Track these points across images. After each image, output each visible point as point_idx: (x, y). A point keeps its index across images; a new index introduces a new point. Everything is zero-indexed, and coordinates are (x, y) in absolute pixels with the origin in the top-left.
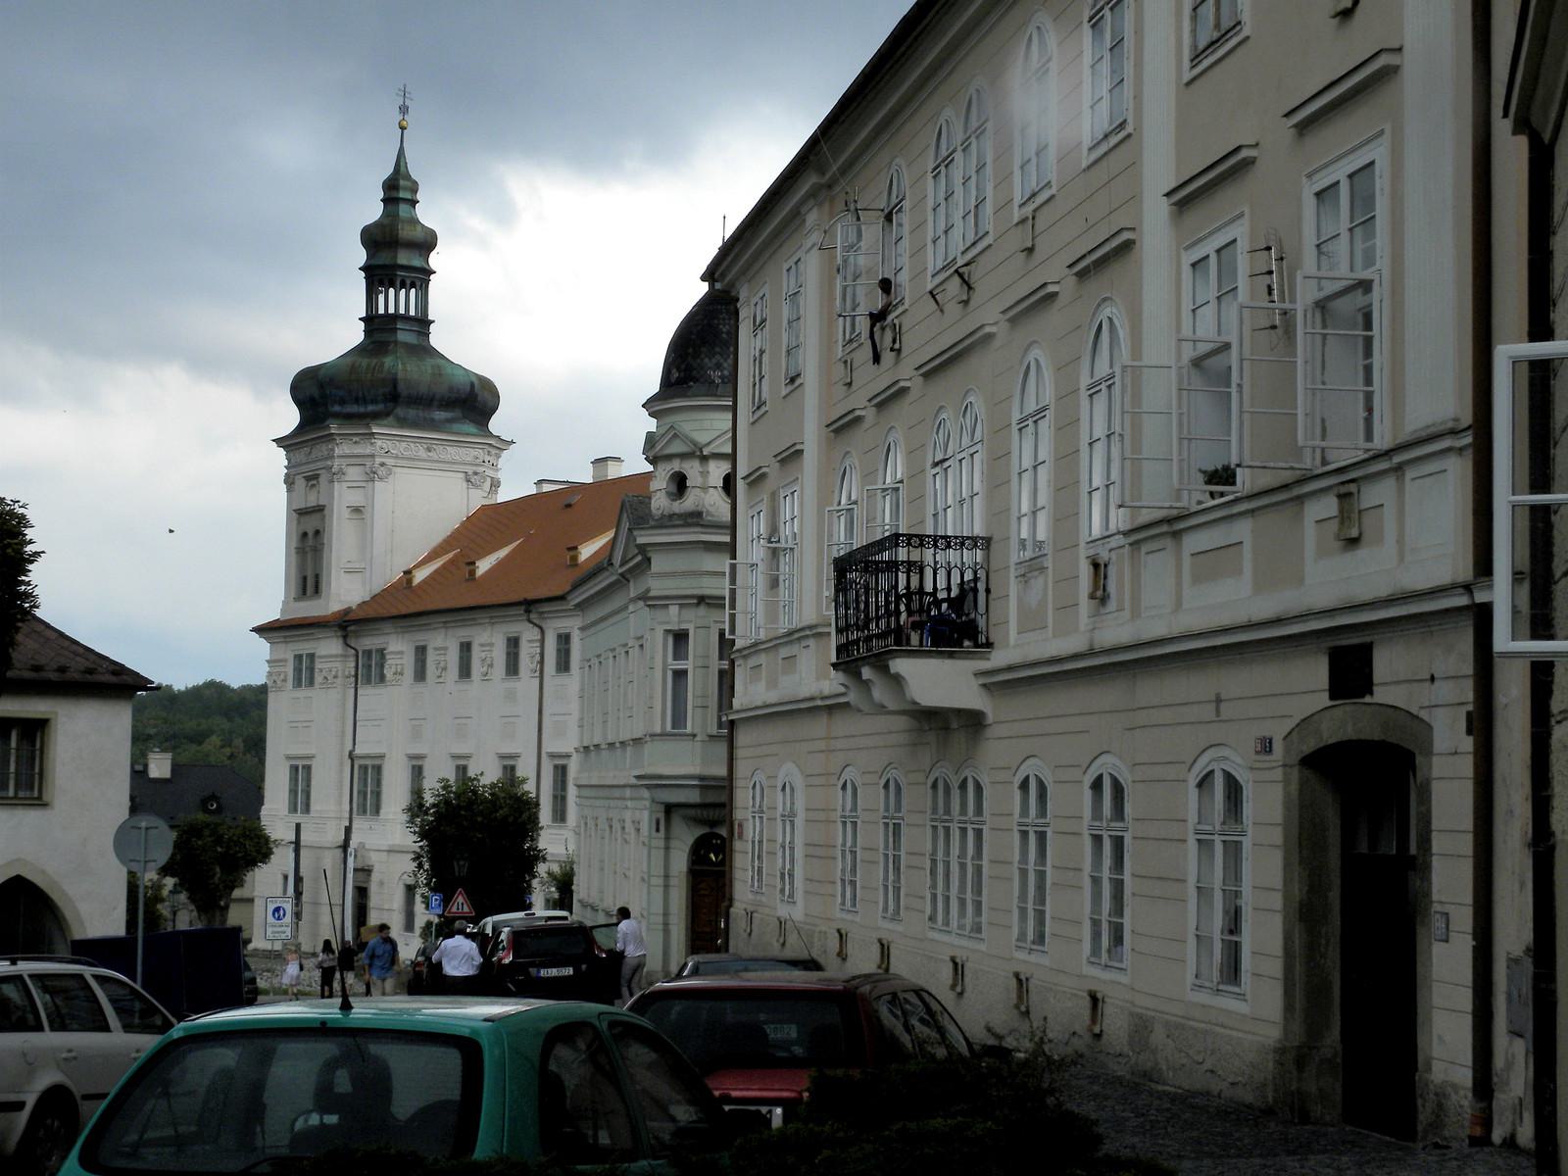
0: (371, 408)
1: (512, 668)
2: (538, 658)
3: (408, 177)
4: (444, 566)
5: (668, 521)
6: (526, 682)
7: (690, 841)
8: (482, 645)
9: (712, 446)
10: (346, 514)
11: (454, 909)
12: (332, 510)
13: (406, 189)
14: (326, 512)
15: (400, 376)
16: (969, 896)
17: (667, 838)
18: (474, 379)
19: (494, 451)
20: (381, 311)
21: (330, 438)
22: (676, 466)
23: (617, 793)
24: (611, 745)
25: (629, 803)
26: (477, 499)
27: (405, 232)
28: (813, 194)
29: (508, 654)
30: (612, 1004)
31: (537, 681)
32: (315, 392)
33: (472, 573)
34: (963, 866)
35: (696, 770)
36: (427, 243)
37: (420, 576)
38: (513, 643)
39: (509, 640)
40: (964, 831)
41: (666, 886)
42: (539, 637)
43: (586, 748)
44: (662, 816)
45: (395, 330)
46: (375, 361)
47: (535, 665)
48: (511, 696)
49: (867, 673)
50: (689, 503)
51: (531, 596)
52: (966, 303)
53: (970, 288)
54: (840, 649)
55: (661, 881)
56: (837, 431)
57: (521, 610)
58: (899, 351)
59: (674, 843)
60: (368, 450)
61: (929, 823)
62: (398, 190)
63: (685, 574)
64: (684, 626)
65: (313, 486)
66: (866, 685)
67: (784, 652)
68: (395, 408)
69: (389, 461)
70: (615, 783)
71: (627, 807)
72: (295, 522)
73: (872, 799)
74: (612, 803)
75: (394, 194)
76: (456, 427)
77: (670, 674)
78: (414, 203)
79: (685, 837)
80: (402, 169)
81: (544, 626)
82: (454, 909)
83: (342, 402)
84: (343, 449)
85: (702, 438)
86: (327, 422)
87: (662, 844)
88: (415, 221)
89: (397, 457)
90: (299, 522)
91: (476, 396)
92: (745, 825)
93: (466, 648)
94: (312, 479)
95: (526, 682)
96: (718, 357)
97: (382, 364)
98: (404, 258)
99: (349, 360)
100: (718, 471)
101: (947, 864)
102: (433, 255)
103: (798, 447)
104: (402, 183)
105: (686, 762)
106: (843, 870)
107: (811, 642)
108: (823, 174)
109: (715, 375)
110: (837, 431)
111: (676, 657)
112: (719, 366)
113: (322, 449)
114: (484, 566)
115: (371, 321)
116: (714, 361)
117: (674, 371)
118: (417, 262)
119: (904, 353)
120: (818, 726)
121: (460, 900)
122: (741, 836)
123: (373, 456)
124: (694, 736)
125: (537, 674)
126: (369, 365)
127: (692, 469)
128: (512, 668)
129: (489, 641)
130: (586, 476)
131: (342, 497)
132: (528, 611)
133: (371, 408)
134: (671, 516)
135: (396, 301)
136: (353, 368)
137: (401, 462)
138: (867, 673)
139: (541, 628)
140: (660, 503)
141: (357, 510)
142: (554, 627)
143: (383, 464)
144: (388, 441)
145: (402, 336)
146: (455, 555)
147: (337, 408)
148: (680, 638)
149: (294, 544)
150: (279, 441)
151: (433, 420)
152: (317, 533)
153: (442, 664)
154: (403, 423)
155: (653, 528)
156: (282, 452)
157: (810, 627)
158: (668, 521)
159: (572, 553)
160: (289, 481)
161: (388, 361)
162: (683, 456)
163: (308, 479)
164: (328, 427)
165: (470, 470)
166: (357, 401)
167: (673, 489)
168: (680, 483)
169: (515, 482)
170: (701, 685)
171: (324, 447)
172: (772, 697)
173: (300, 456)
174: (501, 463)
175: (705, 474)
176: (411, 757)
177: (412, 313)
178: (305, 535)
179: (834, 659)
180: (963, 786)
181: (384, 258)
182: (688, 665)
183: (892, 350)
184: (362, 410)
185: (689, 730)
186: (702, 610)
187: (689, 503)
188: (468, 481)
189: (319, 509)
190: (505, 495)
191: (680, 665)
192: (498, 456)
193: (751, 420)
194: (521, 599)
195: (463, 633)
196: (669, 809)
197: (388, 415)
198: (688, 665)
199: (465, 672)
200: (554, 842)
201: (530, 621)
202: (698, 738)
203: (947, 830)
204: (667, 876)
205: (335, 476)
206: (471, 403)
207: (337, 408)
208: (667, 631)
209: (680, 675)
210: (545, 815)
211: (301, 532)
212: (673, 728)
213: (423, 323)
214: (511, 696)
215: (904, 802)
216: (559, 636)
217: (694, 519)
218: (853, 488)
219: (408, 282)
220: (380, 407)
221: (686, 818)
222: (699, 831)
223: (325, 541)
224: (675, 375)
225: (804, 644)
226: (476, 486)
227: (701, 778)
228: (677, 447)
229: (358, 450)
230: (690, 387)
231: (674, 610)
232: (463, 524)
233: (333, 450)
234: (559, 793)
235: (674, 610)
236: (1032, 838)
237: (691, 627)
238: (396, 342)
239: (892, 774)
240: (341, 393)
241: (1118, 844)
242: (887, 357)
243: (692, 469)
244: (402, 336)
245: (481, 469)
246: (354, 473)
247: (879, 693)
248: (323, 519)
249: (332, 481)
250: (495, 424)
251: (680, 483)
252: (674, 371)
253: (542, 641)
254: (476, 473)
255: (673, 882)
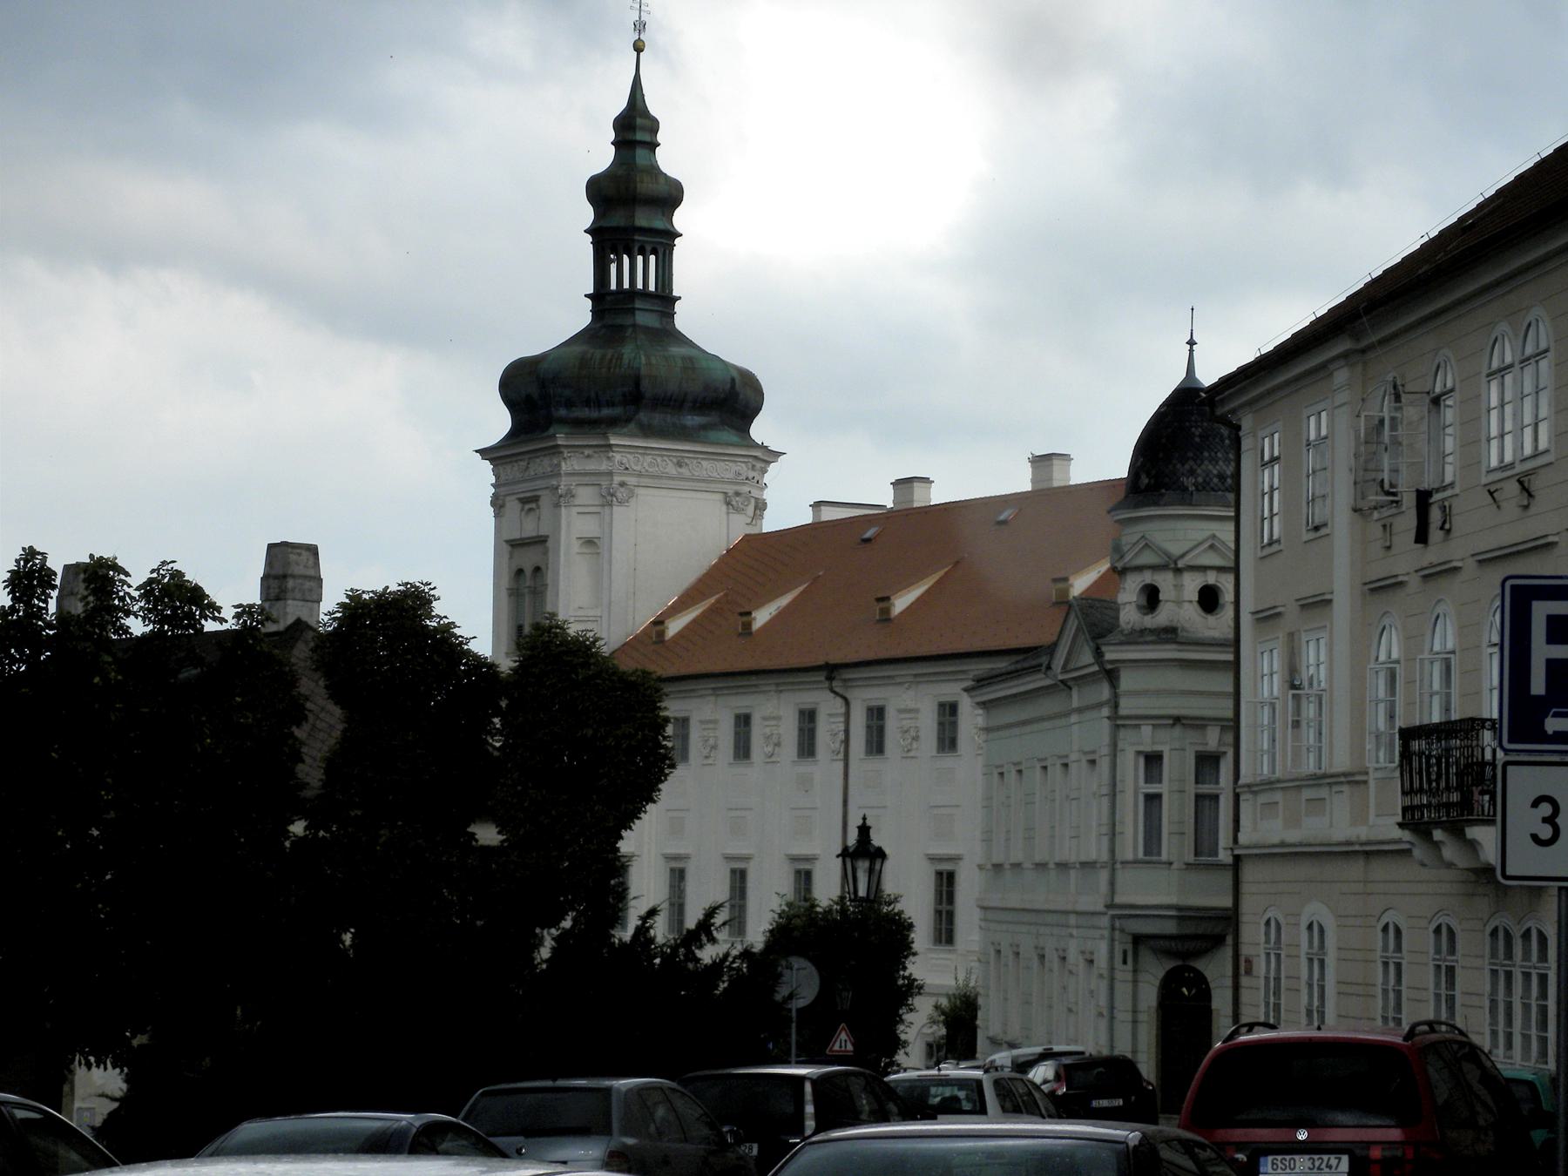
0: (606, 412)
1: (807, 747)
2: (841, 736)
3: (645, 113)
4: (703, 615)
5: (1138, 636)
6: (825, 767)
7: (1161, 974)
8: (765, 719)
9: (1187, 558)
10: (576, 547)
11: (836, 1047)
12: (558, 541)
13: (643, 129)
14: (550, 544)
15: (643, 371)
16: (1534, 1032)
17: (1135, 971)
18: (735, 374)
19: (759, 465)
20: (613, 286)
21: (555, 450)
22: (1147, 578)
23: (1049, 918)
24: (1041, 866)
25: (1074, 932)
26: (739, 529)
27: (645, 186)
28: (1345, 356)
29: (801, 730)
30: (1156, 1123)
31: (841, 765)
32: (534, 391)
33: (747, 626)
34: (1526, 1007)
35: (1173, 900)
36: (671, 196)
37: (674, 627)
38: (808, 718)
39: (802, 713)
40: (1527, 976)
41: (1135, 1022)
42: (843, 710)
43: (998, 867)
44: (1129, 947)
45: (632, 311)
46: (610, 352)
47: (838, 745)
48: (805, 784)
49: (1438, 835)
50: (1162, 617)
51: (835, 658)
52: (1526, 507)
53: (1530, 495)
54: (1405, 810)
55: (1129, 1017)
56: (1373, 590)
57: (821, 677)
58: (1449, 531)
59: (1142, 977)
60: (604, 467)
61: (1488, 968)
62: (635, 129)
63: (1158, 693)
64: (1157, 748)
65: (531, 510)
66: (1437, 846)
67: (1307, 794)
68: (637, 412)
69: (631, 480)
70: (1046, 907)
71: (1071, 936)
72: (506, 556)
73: (1420, 942)
74: (1042, 930)
75: (630, 136)
76: (713, 435)
77: (1141, 798)
78: (653, 145)
79: (1154, 972)
80: (639, 103)
81: (848, 695)
82: (836, 1047)
83: (569, 404)
84: (570, 464)
85: (1175, 549)
86: (551, 431)
87: (1129, 977)
88: (654, 170)
89: (640, 475)
90: (511, 557)
91: (737, 394)
92: (1255, 961)
93: (743, 721)
94: (530, 502)
95: (825, 767)
96: (1191, 463)
97: (620, 357)
98: (643, 219)
99: (577, 349)
100: (1192, 585)
101: (1509, 1006)
102: (678, 213)
103: (1328, 597)
104: (639, 121)
105: (1159, 891)
106: (1385, 1008)
107: (1345, 788)
108: (1358, 340)
109: (1189, 482)
110: (1373, 590)
111: (1149, 779)
112: (1192, 472)
113: (542, 465)
114: (761, 617)
115: (600, 297)
116: (1187, 467)
117: (1143, 476)
118: (659, 224)
119: (1454, 533)
120: (1355, 869)
121: (843, 1036)
122: (1249, 972)
123: (610, 474)
124: (1171, 864)
125: (841, 756)
126: (603, 358)
127: (1164, 581)
128: (807, 747)
129: (776, 714)
130: (887, 499)
131: (574, 524)
132: (830, 678)
133: (606, 412)
134: (1143, 631)
135: (637, 272)
136: (584, 362)
137: (645, 481)
138: (1438, 835)
139: (845, 699)
140: (1130, 616)
141: (590, 542)
142: (862, 698)
143: (622, 484)
144: (629, 453)
145: (642, 319)
146: (718, 601)
147: (563, 412)
148: (1153, 761)
149: (506, 582)
150: (484, 453)
151: (684, 427)
152: (537, 569)
153: (711, 742)
154: (648, 431)
155: (1121, 643)
156: (487, 466)
157: (1345, 775)
158: (1138, 636)
159: (882, 605)
160: (497, 503)
161: (628, 351)
162: (1154, 568)
163: (524, 501)
164: (553, 437)
165: (730, 489)
166: (587, 403)
167: (1143, 602)
168: (1151, 598)
169: (787, 504)
170: (1176, 813)
171: (546, 461)
172: (1293, 836)
173: (513, 471)
174: (767, 478)
175: (1179, 587)
176: (670, 858)
177: (652, 288)
178: (520, 572)
179: (1400, 819)
180: (1526, 935)
181: (617, 219)
182: (1163, 788)
183: (1442, 528)
184: (595, 414)
185: (1164, 857)
186: (1177, 731)
187: (1162, 617)
188: (728, 504)
189: (541, 541)
190: (772, 522)
191: (1153, 789)
192: (764, 471)
193: (1260, 554)
194: (821, 662)
195: (742, 703)
196: (1138, 940)
197: (628, 420)
198: (1163, 788)
199: (742, 750)
200: (934, 971)
201: (833, 691)
202: (1175, 866)
203: (1509, 975)
204: (1135, 1012)
205: (561, 499)
206: (723, 405)
207: (563, 412)
208: (1139, 753)
209: (1153, 800)
210: (921, 937)
211: (515, 569)
212: (1146, 854)
213: (665, 300)
214: (805, 784)
215: (1459, 946)
216: (870, 710)
217: (1169, 634)
218: (1392, 646)
219: (648, 248)
220: (617, 411)
221: (1155, 951)
222: (1170, 964)
223: (549, 581)
224: (1145, 480)
225: (1335, 788)
226: (738, 510)
227: (1179, 908)
228: (1147, 558)
229: (591, 466)
230: (1162, 495)
231: (1146, 730)
232: (722, 559)
233: (559, 465)
234: (944, 907)
235: (1146, 730)
236: (1392, 968)
237: (1165, 750)
238: (634, 326)
239: (1442, 920)
240: (567, 392)
241: (1398, 966)
242: (1435, 535)
243: (1164, 581)
244: (642, 319)
245: (745, 489)
246: (585, 495)
247: (1449, 852)
248: (546, 553)
249: (557, 505)
250: (760, 430)
251: (1151, 598)
252: (1143, 476)
253: (847, 715)
254: (737, 494)
255: (1143, 1017)
